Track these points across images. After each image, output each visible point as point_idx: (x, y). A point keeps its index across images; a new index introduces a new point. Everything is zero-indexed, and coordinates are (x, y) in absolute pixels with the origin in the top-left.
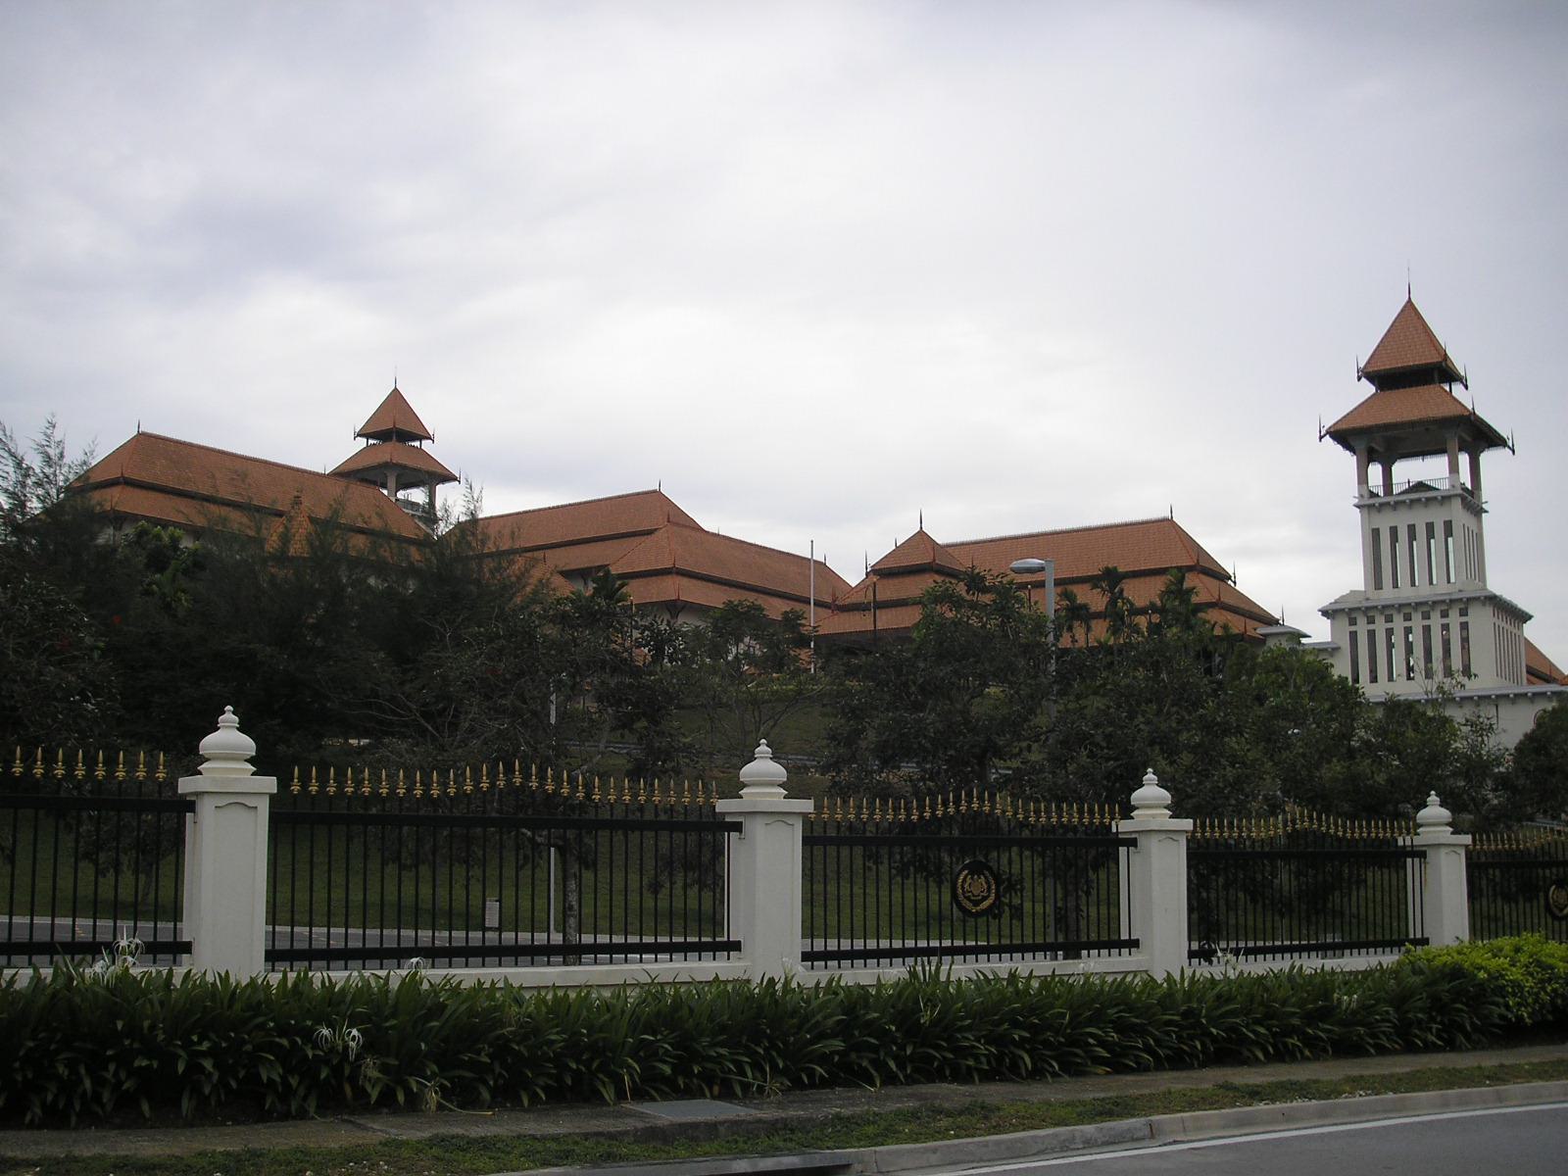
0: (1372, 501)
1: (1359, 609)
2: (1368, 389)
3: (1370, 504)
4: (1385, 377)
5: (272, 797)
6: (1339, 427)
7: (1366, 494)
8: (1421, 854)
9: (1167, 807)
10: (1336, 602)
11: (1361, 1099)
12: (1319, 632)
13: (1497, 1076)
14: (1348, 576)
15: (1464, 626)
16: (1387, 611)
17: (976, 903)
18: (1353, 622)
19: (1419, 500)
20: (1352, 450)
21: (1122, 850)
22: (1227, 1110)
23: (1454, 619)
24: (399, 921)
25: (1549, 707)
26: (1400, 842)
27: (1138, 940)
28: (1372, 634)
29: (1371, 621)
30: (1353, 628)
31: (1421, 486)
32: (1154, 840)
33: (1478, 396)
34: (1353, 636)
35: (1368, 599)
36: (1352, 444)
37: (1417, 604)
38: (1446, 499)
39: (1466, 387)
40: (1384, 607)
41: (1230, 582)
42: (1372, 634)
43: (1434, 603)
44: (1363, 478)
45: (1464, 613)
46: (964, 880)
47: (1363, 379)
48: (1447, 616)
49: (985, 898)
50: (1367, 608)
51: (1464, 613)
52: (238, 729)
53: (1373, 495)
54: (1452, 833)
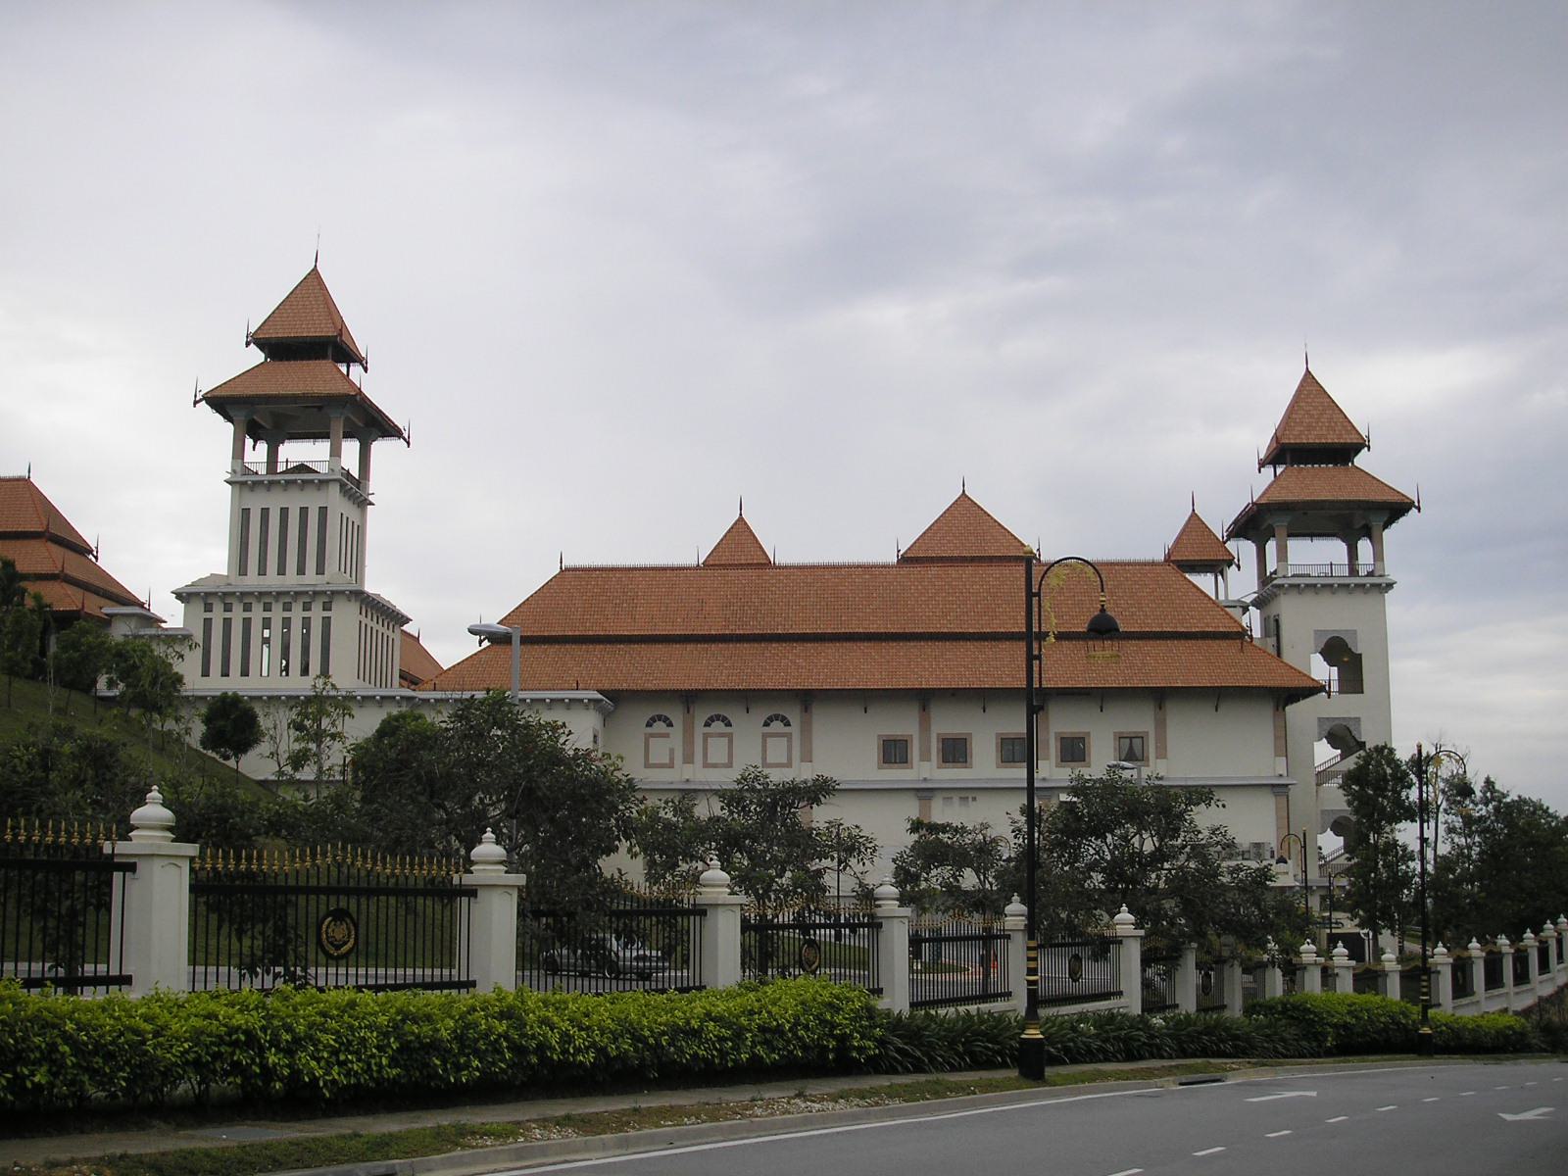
0: (244, 478)
1: (216, 594)
2: (257, 356)
3: (243, 482)
4: (277, 345)
5: (520, 889)
6: (216, 393)
7: (238, 469)
8: (471, 892)
9: (501, 863)
10: (193, 584)
11: (896, 1104)
12: (173, 615)
13: (620, 1122)
14: (212, 559)
15: (326, 622)
16: (246, 598)
17: (338, 948)
18: (208, 608)
19: (294, 482)
20: (229, 418)
21: (117, 876)
22: (990, 1094)
23: (317, 614)
24: (96, 958)
25: (395, 712)
26: (456, 881)
27: (475, 982)
28: (227, 623)
29: (228, 608)
30: (208, 615)
31: (302, 468)
32: (157, 864)
33: (375, 384)
34: (208, 622)
35: (229, 584)
36: (231, 414)
37: (260, 593)
38: (324, 483)
39: (366, 370)
40: (243, 594)
41: (91, 557)
42: (227, 623)
43: (297, 593)
44: (238, 452)
45: (327, 607)
46: (328, 927)
47: (252, 344)
48: (310, 609)
49: (345, 943)
50: (225, 594)
51: (327, 607)
52: (162, 804)
53: (247, 471)
54: (506, 872)
